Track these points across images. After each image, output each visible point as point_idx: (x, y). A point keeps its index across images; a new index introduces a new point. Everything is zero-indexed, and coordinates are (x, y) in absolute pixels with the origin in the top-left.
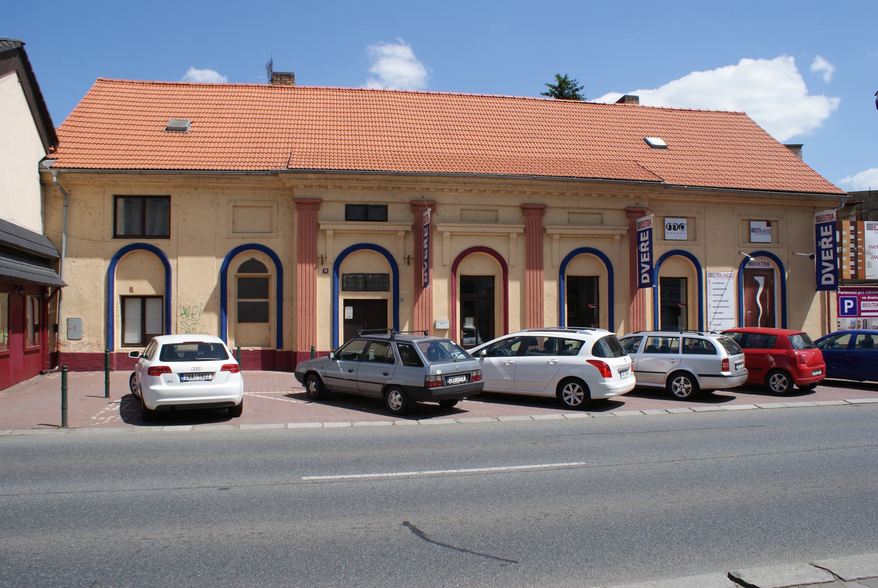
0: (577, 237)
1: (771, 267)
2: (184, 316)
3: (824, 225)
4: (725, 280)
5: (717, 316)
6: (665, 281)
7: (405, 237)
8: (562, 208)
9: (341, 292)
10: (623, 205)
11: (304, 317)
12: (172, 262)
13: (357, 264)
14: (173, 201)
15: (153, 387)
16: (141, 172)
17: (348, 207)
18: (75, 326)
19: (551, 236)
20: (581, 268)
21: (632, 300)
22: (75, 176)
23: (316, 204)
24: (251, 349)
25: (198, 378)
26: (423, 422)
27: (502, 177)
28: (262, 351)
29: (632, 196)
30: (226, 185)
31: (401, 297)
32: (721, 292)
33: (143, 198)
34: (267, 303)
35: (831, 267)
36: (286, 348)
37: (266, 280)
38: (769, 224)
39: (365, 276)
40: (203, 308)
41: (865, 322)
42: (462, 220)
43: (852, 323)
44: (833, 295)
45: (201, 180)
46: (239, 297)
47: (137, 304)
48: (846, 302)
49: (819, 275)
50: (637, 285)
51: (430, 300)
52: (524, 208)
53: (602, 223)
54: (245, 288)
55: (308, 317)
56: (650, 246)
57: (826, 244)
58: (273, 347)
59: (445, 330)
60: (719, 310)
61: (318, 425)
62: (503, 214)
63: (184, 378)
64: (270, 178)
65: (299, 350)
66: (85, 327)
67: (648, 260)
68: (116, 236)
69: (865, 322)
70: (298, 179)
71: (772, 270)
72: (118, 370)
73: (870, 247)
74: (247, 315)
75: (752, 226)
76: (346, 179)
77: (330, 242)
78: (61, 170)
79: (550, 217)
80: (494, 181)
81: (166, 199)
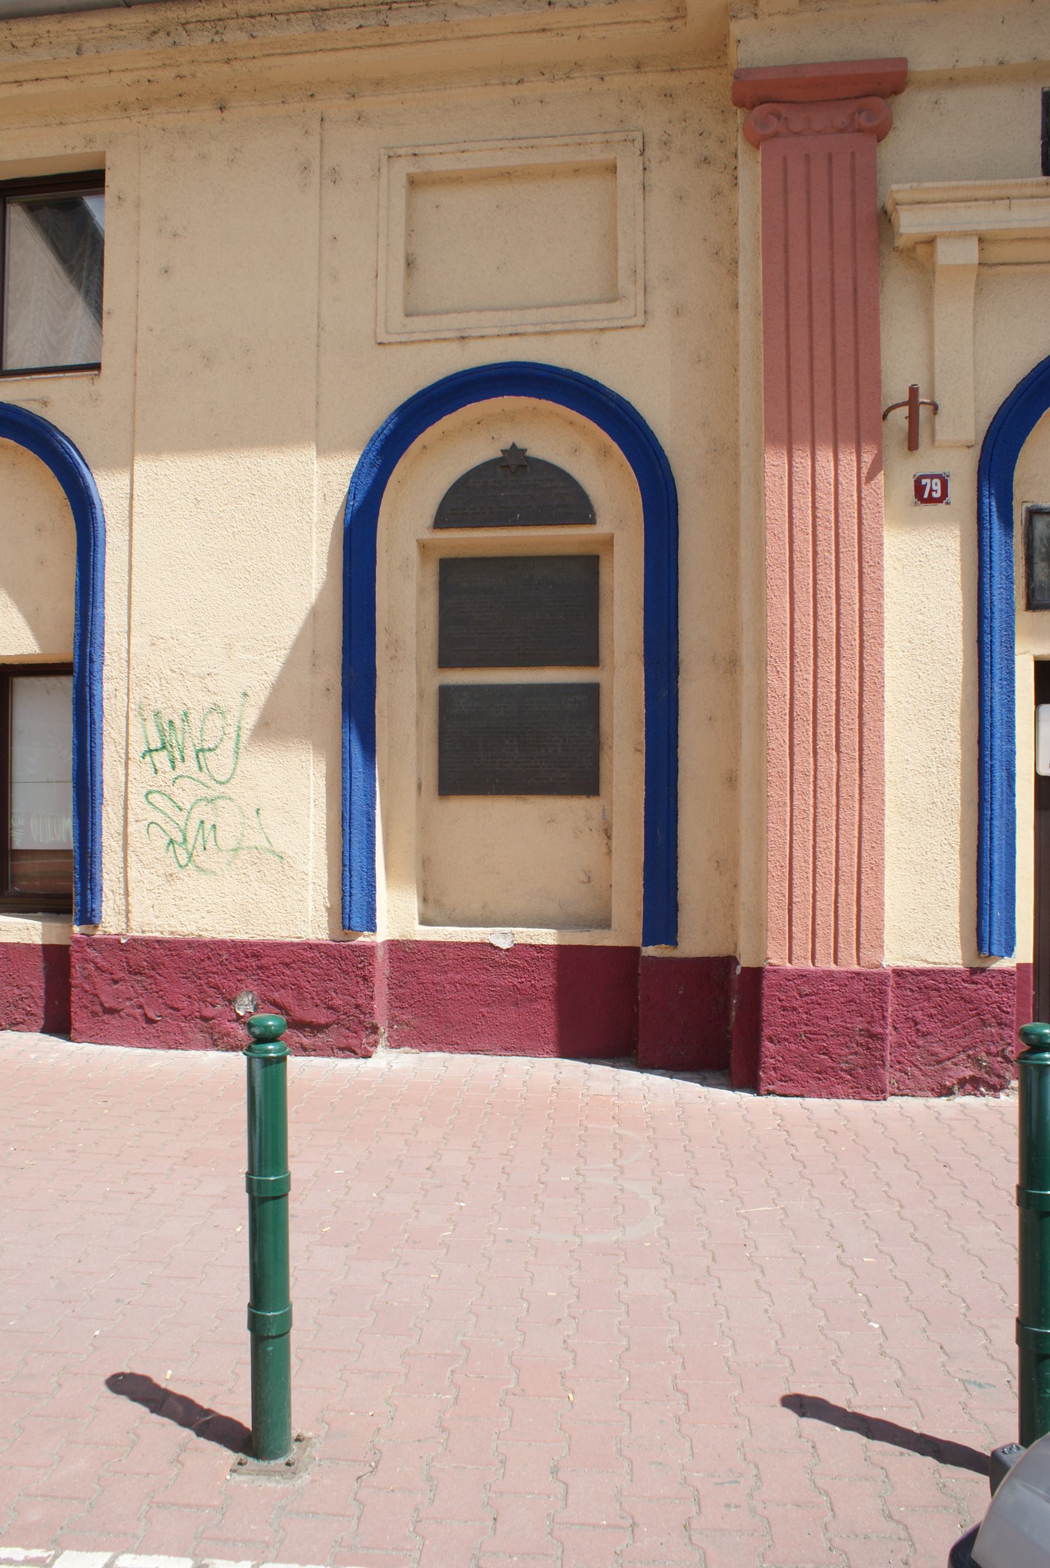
2: (161, 759)
9: (1023, 619)
11: (804, 760)
12: (107, 488)
24: (502, 938)
28: (563, 952)
34: (592, 691)
36: (695, 941)
37: (588, 567)
40: (251, 717)
46: (446, 660)
54: (479, 610)
55: (828, 765)
58: (625, 929)
65: (776, 957)
74: (496, 751)
77: (954, 313)
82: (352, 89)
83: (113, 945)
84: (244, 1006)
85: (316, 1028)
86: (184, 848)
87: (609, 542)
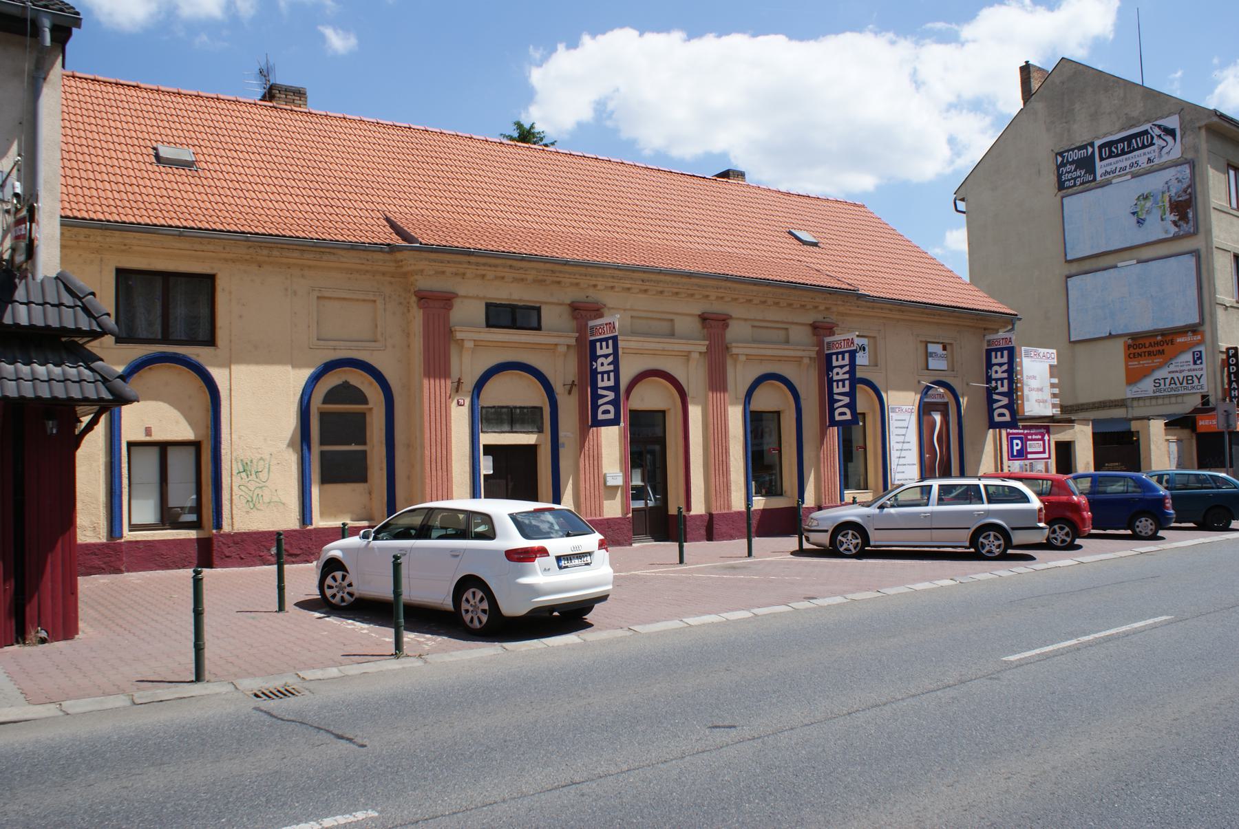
0: (762, 359)
1: (946, 400)
2: (244, 475)
3: (996, 350)
4: (906, 417)
5: (902, 461)
6: (635, 415)
7: (565, 356)
8: (746, 320)
10: (810, 318)
11: (434, 473)
12: (884, 395)
13: (513, 391)
14: (221, 284)
15: (524, 580)
16: (182, 232)
20: (767, 399)
21: (822, 443)
23: (446, 300)
25: (576, 562)
26: (510, 645)
27: (690, 275)
29: (822, 308)
30: (311, 263)
31: (561, 440)
32: (903, 432)
33: (166, 276)
35: (1005, 401)
38: (944, 349)
39: (511, 409)
41: (1031, 464)
42: (754, 341)
43: (1021, 467)
44: (1004, 432)
45: (275, 253)
47: (153, 456)
51: (599, 446)
52: (704, 318)
53: (787, 342)
55: (440, 473)
56: (616, 363)
57: (999, 373)
59: (617, 487)
61: (675, 624)
63: (563, 563)
64: (380, 256)
67: (611, 383)
69: (1031, 464)
71: (946, 404)
73: (1029, 377)
77: (466, 358)
79: (735, 331)
80: (677, 279)
81: (211, 279)
82: (302, 267)
83: (228, 535)
85: (297, 555)
86: (252, 504)
87: (371, 409)
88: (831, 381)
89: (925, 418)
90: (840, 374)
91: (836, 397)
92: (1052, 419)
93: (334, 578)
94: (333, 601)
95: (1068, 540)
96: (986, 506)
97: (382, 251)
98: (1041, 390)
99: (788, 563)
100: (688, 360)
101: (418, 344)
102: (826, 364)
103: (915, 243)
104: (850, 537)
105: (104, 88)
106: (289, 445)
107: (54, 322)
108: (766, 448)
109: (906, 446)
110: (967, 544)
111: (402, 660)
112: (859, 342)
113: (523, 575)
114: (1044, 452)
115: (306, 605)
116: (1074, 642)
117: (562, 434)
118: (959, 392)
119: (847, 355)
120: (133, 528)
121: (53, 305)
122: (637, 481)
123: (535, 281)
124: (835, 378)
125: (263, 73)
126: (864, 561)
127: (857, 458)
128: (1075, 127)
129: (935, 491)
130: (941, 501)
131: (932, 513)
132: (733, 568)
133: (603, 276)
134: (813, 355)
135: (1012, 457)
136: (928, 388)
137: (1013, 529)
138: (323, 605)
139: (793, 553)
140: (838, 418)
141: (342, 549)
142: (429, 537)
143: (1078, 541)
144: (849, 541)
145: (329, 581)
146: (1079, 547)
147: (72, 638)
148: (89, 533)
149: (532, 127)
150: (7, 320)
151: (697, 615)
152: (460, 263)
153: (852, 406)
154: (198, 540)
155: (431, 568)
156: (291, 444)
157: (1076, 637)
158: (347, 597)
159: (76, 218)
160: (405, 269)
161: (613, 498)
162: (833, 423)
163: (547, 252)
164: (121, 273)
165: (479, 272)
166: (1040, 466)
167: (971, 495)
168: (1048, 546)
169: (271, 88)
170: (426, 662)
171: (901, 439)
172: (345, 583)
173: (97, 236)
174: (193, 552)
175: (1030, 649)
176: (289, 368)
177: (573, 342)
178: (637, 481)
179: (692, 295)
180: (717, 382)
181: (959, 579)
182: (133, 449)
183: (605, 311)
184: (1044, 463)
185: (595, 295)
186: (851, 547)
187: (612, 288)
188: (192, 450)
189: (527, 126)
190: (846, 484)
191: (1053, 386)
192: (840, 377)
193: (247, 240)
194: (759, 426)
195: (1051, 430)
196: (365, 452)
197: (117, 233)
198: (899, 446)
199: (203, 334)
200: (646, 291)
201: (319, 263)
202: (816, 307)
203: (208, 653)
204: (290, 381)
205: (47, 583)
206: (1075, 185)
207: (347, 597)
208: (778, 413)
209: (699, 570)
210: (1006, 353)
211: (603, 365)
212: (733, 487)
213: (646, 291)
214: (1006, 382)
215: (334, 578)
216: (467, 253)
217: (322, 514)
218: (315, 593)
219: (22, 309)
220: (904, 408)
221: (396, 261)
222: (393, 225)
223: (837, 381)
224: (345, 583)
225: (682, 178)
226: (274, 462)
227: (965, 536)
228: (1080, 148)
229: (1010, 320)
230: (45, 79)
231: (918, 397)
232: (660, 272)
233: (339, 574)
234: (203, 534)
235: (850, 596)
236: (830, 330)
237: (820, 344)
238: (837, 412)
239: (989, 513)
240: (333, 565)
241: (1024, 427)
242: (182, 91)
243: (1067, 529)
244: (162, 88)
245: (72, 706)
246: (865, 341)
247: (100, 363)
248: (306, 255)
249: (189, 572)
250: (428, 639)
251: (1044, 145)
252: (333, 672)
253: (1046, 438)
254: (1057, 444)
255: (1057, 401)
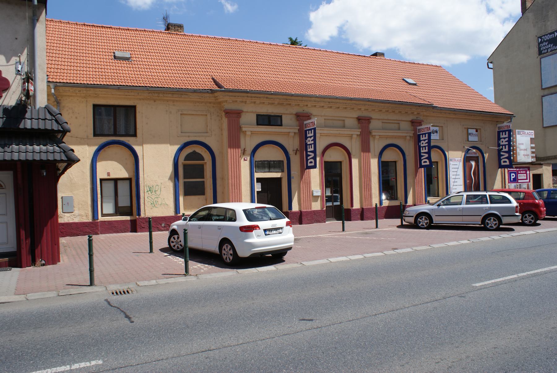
0: (387, 137)
1: (477, 155)
2: (149, 192)
3: (503, 131)
4: (458, 163)
5: (455, 184)
7: (293, 137)
8: (379, 119)
9: (255, 174)
10: (411, 118)
11: (233, 190)
12: (446, 153)
14: (138, 109)
16: (119, 88)
17: (258, 116)
18: (69, 202)
19: (374, 137)
20: (389, 156)
21: (302, 178)
22: (67, 89)
23: (238, 113)
25: (274, 232)
26: (240, 271)
27: (351, 99)
29: (415, 113)
30: (177, 99)
31: (292, 175)
32: (456, 170)
33: (115, 107)
35: (507, 155)
38: (477, 131)
39: (269, 162)
42: (383, 129)
43: (515, 186)
44: (506, 170)
45: (161, 95)
47: (111, 185)
48: (512, 174)
49: (500, 160)
50: (306, 167)
52: (359, 119)
53: (399, 129)
55: (236, 191)
56: (314, 140)
57: (504, 142)
59: (318, 196)
60: (456, 180)
62: (348, 122)
63: (267, 233)
64: (208, 95)
66: (76, 204)
67: (312, 149)
68: (95, 135)
70: (229, 96)
71: (478, 157)
72: (101, 234)
73: (519, 144)
75: (469, 132)
76: (260, 98)
78: (58, 84)
79: (374, 124)
80: (345, 101)
81: (134, 107)
82: (173, 101)
83: (143, 218)
84: (163, 225)
86: (154, 205)
88: (420, 147)
89: (467, 164)
90: (424, 144)
91: (422, 154)
92: (532, 163)
93: (174, 238)
94: (174, 248)
95: (533, 221)
96: (489, 205)
97: (208, 92)
98: (526, 150)
99: (393, 231)
100: (352, 138)
101: (225, 133)
102: (417, 139)
103: (465, 82)
104: (423, 219)
105: (96, 29)
106: (169, 179)
107: (42, 127)
108: (390, 178)
109: (457, 177)
110: (480, 223)
111: (187, 277)
112: (432, 128)
113: (247, 238)
114: (527, 179)
115: (163, 250)
116: (515, 276)
117: (292, 173)
118: (484, 151)
119: (427, 135)
120: (103, 215)
121: (42, 120)
122: (329, 194)
123: (278, 104)
124: (422, 145)
125: (165, 19)
126: (430, 230)
127: (433, 182)
128: (549, 23)
129: (465, 197)
130: (468, 202)
131: (463, 208)
132: (366, 233)
133: (310, 101)
134: (412, 135)
135: (510, 181)
136: (469, 150)
137: (503, 216)
138: (170, 250)
139: (398, 227)
140: (423, 164)
141: (178, 226)
142: (212, 220)
143: (538, 222)
144: (423, 221)
145: (172, 239)
146: (539, 224)
147: (56, 263)
148: (84, 218)
149: (296, 39)
150: (22, 126)
151: (337, 257)
152: (243, 97)
153: (429, 158)
154: (131, 220)
155: (206, 236)
156: (170, 179)
157: (517, 273)
158: (180, 246)
159: (74, 83)
160: (220, 100)
161: (317, 201)
162: (421, 166)
163: (284, 91)
164: (95, 106)
165: (253, 101)
166: (525, 186)
167: (483, 200)
168: (522, 224)
169: (168, 25)
170: (198, 278)
171: (455, 173)
172: (179, 240)
173: (84, 91)
174: (129, 226)
175: (490, 280)
176: (169, 145)
177: (297, 131)
178: (329, 194)
179: (353, 109)
180: (365, 148)
181: (472, 240)
182: (103, 182)
183: (312, 117)
184: (525, 183)
185: (307, 110)
186: (424, 224)
187: (315, 106)
188: (128, 182)
189: (294, 39)
190: (429, 193)
191: (532, 148)
192: (424, 145)
193: (148, 90)
194: (386, 169)
195: (531, 169)
196: (204, 182)
197: (92, 89)
198: (454, 177)
199: (132, 132)
200: (331, 107)
201: (181, 99)
202: (413, 113)
203: (96, 274)
204: (168, 151)
205: (44, 240)
206: (547, 52)
207: (180, 246)
208: (395, 162)
209: (349, 235)
210: (507, 132)
211: (310, 141)
212: (373, 196)
213: (331, 107)
214: (507, 146)
215: (174, 238)
216: (246, 92)
217: (185, 209)
218: (166, 245)
219: (29, 122)
220: (456, 159)
221: (215, 97)
222: (215, 81)
223: (423, 147)
224: (179, 240)
225: (360, 58)
226: (162, 187)
227: (478, 220)
228: (550, 34)
229: (509, 117)
230: (38, 20)
231: (464, 153)
232: (337, 98)
233: (176, 236)
234: (133, 218)
235: (415, 248)
236: (420, 123)
237: (415, 130)
238: (423, 161)
239: (491, 208)
240: (174, 232)
241: (516, 168)
242: (130, 28)
243: (532, 216)
244: (121, 27)
245: (31, 296)
246: (437, 128)
247: (63, 144)
248: (175, 96)
249: (87, 237)
250: (205, 267)
251: (532, 33)
252: (153, 282)
253: (528, 172)
254: (534, 175)
255: (534, 155)
